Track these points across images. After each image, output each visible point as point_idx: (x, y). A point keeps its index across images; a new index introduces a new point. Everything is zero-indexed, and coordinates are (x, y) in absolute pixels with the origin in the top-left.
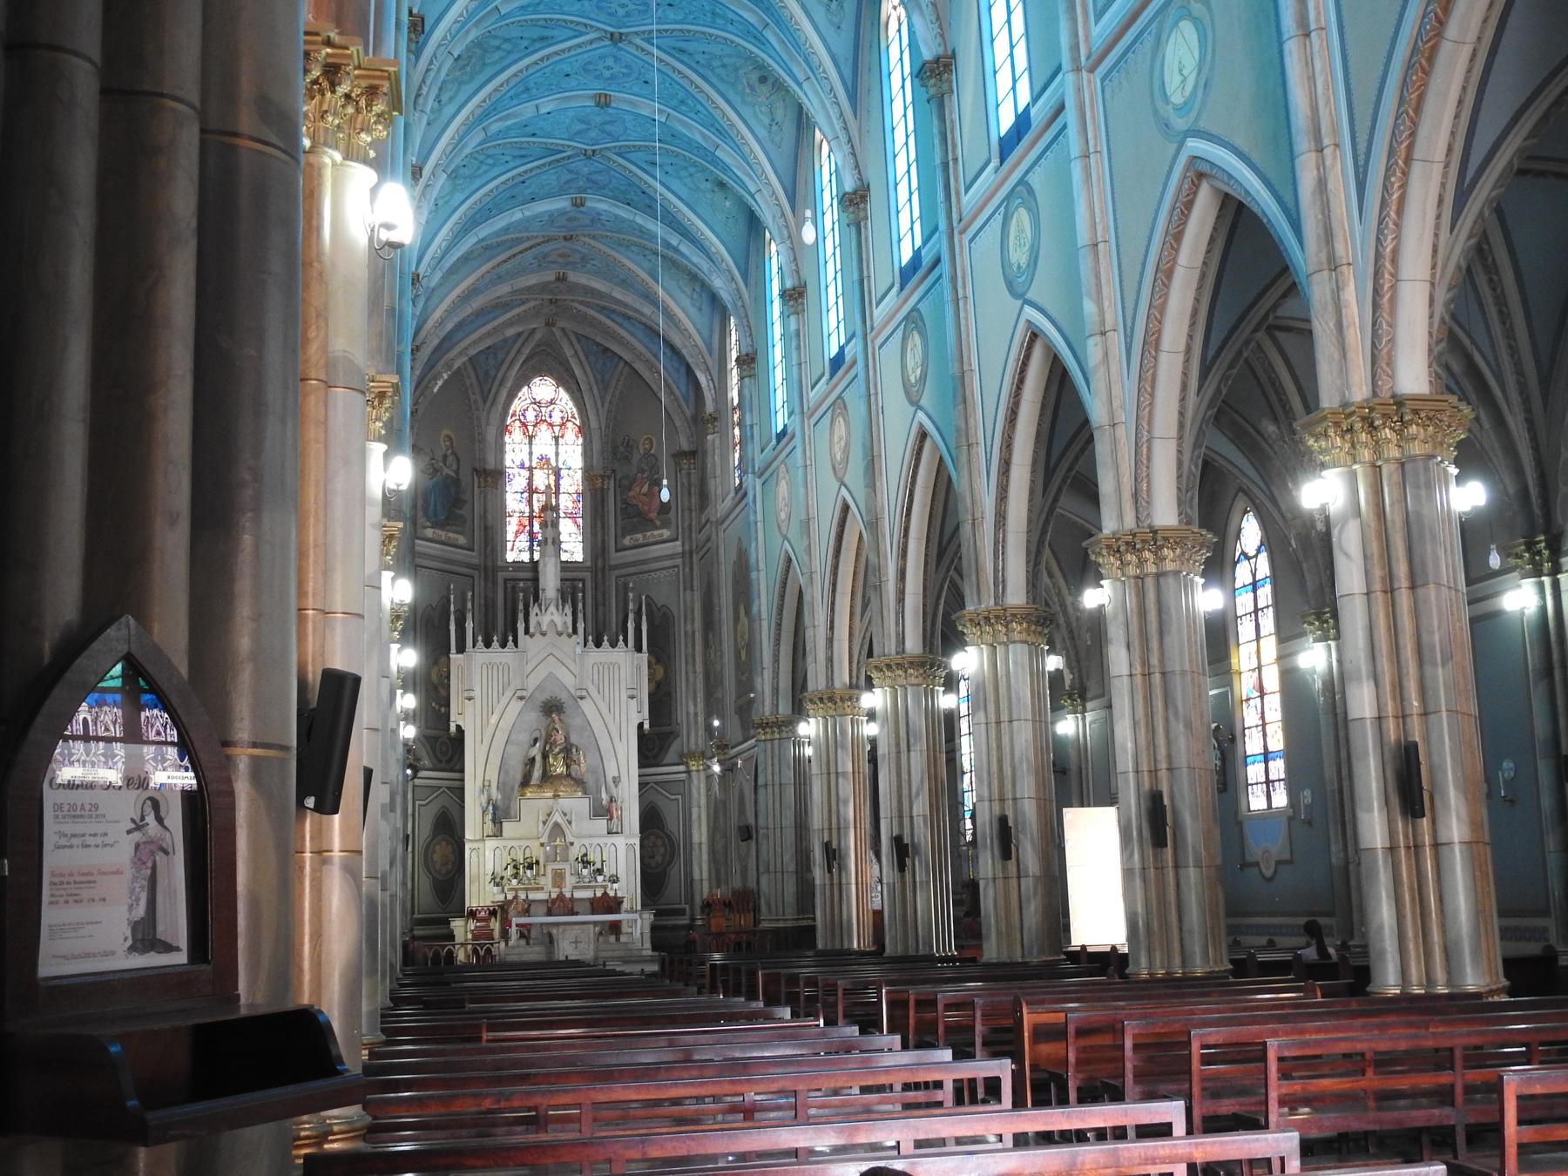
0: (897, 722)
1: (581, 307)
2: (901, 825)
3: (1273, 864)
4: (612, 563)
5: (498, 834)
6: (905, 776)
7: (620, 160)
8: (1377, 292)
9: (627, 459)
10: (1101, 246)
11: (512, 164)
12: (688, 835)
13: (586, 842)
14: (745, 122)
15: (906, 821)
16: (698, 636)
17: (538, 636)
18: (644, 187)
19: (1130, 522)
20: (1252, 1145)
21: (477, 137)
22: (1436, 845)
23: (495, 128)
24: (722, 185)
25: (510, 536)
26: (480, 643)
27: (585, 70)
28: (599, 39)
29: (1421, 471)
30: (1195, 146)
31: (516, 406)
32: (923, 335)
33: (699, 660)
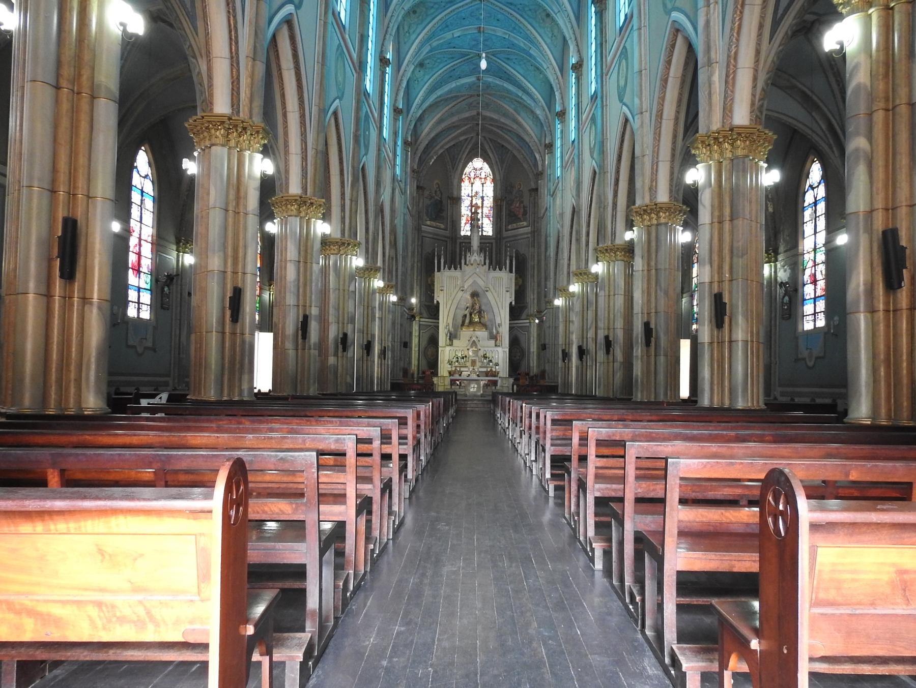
0: (583, 298)
3: (814, 359)
4: (504, 236)
5: (451, 345)
6: (585, 321)
7: (494, 58)
8: (727, 76)
10: (643, 72)
12: (529, 349)
13: (486, 349)
14: (540, 36)
15: (585, 340)
16: (536, 266)
18: (505, 70)
19: (647, 201)
21: (427, 49)
22: (731, 342)
23: (435, 44)
24: (538, 69)
25: (463, 225)
26: (446, 268)
27: (472, 16)
29: (741, 163)
30: (675, 15)
31: (467, 170)
32: (595, 125)
33: (536, 276)
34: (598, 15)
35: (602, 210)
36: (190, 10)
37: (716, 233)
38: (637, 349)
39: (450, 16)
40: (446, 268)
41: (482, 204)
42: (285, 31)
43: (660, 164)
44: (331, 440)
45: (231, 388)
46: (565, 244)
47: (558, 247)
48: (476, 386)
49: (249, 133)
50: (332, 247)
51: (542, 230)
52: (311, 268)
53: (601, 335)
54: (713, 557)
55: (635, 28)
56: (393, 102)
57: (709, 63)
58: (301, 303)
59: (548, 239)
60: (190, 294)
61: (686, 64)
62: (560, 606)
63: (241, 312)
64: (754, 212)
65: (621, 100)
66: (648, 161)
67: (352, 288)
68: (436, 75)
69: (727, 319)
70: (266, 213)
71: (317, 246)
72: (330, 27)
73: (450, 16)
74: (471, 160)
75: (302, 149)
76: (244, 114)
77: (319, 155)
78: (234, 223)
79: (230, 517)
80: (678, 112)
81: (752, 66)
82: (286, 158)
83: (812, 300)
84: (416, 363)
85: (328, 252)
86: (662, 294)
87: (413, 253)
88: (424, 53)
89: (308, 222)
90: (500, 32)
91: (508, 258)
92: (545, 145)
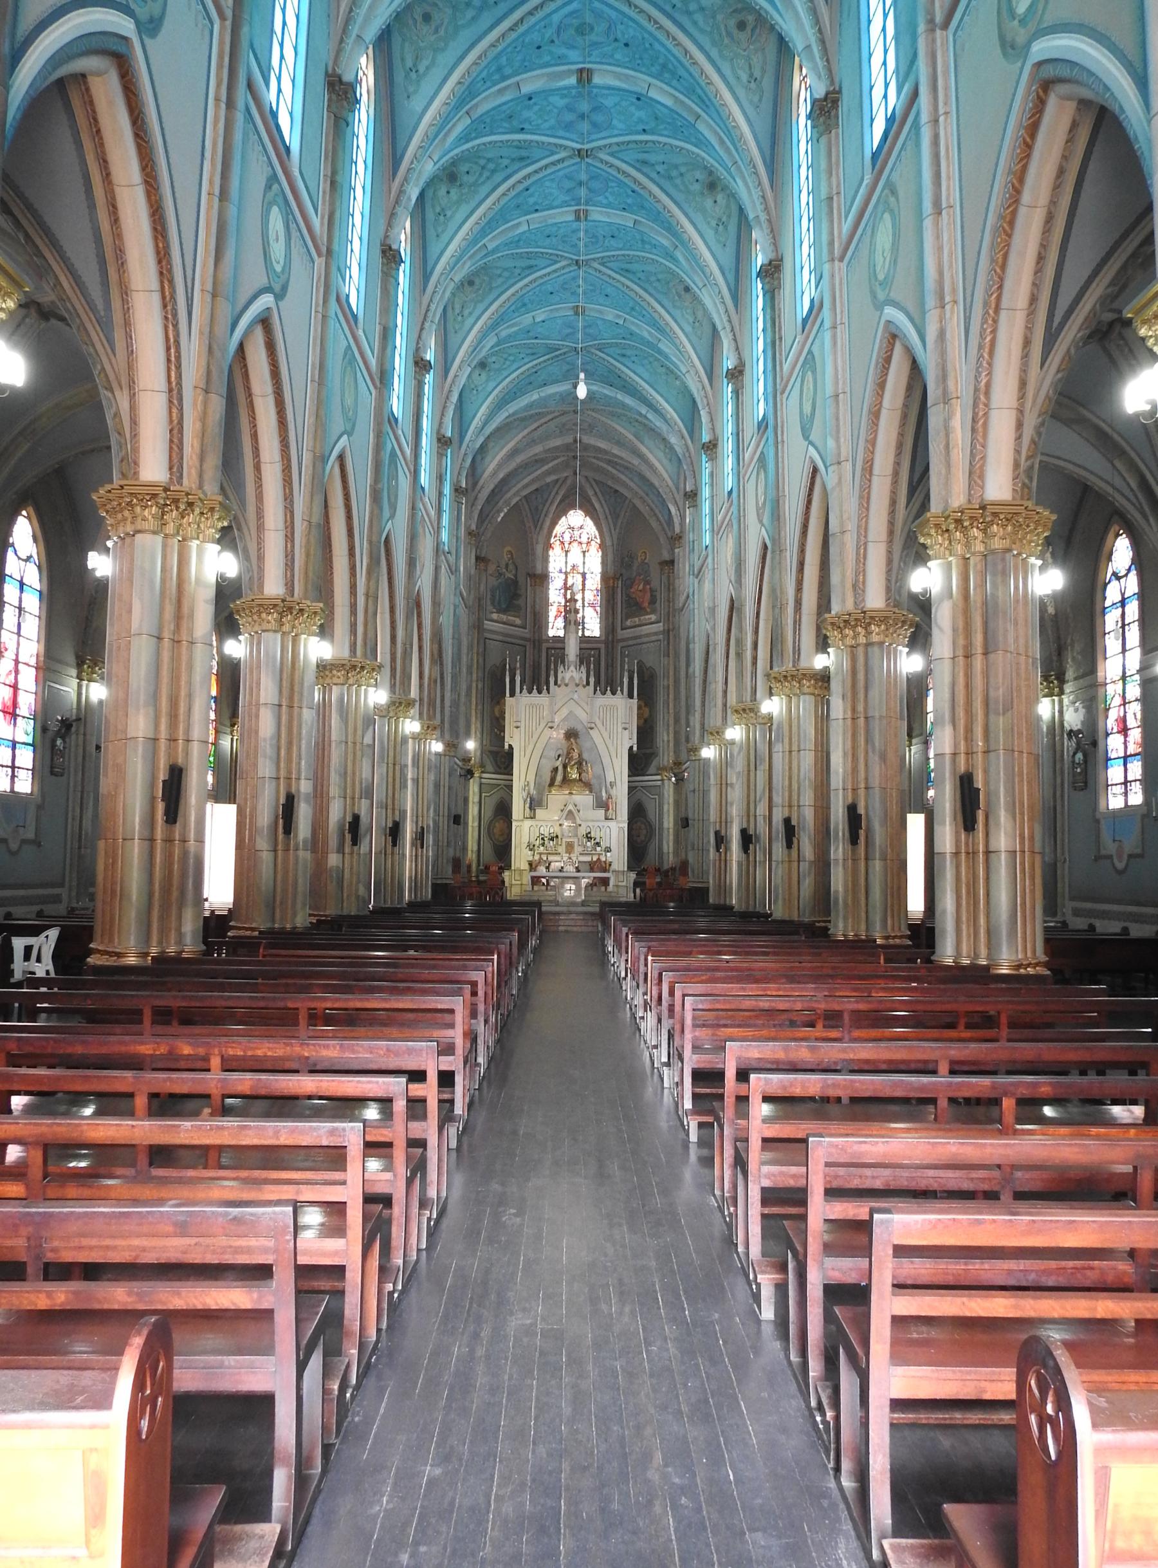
1: (594, 461)
2: (748, 821)
3: (1125, 857)
4: (619, 637)
5: (533, 817)
6: (752, 787)
8: (974, 420)
9: (629, 566)
10: (841, 396)
11: (526, 360)
13: (590, 824)
14: (676, 321)
16: (671, 688)
17: (563, 687)
19: (850, 606)
20: (364, 1086)
21: (491, 340)
22: (987, 852)
23: (504, 334)
24: (672, 372)
25: (551, 619)
26: (525, 691)
28: (569, 265)
30: (890, 312)
31: (558, 529)
32: (765, 472)
33: (671, 705)
34: (768, 296)
35: (777, 611)
36: (102, 313)
37: (961, 674)
38: (837, 849)
39: (528, 289)
40: (525, 691)
41: (584, 585)
42: (259, 335)
43: (870, 546)
44: (322, 1132)
45: (164, 932)
46: (718, 657)
47: (707, 661)
48: (573, 887)
49: (197, 511)
50: (335, 672)
51: (682, 630)
52: (300, 715)
53: (778, 816)
54: (950, 1375)
55: (827, 324)
56: (436, 427)
57: (946, 399)
58: (283, 774)
59: (691, 646)
60: (98, 748)
61: (909, 388)
62: (702, 1413)
63: (182, 802)
64: (1022, 641)
65: (806, 437)
66: (850, 541)
67: (368, 740)
68: (508, 380)
69: (980, 816)
70: (227, 625)
71: (310, 675)
72: (332, 323)
73: (528, 289)
74: (564, 512)
75: (286, 522)
76: (189, 481)
77: (314, 531)
78: (172, 659)
79: (139, 1433)
80: (897, 464)
81: (1015, 404)
82: (259, 537)
83: (1122, 761)
84: (475, 848)
85: (328, 681)
86: (877, 758)
87: (470, 668)
88: (489, 346)
89: (295, 640)
90: (610, 314)
91: (626, 674)
92: (686, 494)
